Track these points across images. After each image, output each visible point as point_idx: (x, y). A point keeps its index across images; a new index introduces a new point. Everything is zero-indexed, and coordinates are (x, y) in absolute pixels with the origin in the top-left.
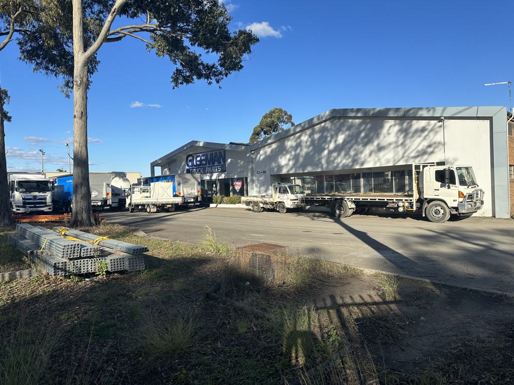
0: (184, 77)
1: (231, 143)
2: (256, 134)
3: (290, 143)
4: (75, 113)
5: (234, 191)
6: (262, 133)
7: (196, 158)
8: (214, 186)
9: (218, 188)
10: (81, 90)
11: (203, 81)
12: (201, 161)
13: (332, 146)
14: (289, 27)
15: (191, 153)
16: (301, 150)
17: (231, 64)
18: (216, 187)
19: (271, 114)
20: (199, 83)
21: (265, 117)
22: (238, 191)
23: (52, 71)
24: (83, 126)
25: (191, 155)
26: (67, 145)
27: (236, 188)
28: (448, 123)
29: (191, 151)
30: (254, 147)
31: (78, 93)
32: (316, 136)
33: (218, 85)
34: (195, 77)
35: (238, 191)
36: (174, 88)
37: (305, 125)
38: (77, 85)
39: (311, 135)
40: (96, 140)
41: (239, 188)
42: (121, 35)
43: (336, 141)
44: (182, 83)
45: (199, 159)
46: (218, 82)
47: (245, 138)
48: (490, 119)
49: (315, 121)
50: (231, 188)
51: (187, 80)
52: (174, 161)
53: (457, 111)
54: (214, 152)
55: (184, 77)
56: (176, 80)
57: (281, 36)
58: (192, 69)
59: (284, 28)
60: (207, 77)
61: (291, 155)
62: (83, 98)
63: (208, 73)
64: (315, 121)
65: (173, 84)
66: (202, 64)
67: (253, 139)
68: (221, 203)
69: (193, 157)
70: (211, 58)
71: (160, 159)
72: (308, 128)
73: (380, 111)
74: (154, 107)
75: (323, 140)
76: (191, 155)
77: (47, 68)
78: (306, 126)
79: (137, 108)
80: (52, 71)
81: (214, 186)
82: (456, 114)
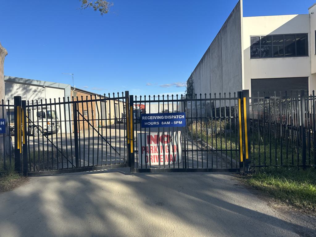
28: (47, 89)
48: (64, 89)
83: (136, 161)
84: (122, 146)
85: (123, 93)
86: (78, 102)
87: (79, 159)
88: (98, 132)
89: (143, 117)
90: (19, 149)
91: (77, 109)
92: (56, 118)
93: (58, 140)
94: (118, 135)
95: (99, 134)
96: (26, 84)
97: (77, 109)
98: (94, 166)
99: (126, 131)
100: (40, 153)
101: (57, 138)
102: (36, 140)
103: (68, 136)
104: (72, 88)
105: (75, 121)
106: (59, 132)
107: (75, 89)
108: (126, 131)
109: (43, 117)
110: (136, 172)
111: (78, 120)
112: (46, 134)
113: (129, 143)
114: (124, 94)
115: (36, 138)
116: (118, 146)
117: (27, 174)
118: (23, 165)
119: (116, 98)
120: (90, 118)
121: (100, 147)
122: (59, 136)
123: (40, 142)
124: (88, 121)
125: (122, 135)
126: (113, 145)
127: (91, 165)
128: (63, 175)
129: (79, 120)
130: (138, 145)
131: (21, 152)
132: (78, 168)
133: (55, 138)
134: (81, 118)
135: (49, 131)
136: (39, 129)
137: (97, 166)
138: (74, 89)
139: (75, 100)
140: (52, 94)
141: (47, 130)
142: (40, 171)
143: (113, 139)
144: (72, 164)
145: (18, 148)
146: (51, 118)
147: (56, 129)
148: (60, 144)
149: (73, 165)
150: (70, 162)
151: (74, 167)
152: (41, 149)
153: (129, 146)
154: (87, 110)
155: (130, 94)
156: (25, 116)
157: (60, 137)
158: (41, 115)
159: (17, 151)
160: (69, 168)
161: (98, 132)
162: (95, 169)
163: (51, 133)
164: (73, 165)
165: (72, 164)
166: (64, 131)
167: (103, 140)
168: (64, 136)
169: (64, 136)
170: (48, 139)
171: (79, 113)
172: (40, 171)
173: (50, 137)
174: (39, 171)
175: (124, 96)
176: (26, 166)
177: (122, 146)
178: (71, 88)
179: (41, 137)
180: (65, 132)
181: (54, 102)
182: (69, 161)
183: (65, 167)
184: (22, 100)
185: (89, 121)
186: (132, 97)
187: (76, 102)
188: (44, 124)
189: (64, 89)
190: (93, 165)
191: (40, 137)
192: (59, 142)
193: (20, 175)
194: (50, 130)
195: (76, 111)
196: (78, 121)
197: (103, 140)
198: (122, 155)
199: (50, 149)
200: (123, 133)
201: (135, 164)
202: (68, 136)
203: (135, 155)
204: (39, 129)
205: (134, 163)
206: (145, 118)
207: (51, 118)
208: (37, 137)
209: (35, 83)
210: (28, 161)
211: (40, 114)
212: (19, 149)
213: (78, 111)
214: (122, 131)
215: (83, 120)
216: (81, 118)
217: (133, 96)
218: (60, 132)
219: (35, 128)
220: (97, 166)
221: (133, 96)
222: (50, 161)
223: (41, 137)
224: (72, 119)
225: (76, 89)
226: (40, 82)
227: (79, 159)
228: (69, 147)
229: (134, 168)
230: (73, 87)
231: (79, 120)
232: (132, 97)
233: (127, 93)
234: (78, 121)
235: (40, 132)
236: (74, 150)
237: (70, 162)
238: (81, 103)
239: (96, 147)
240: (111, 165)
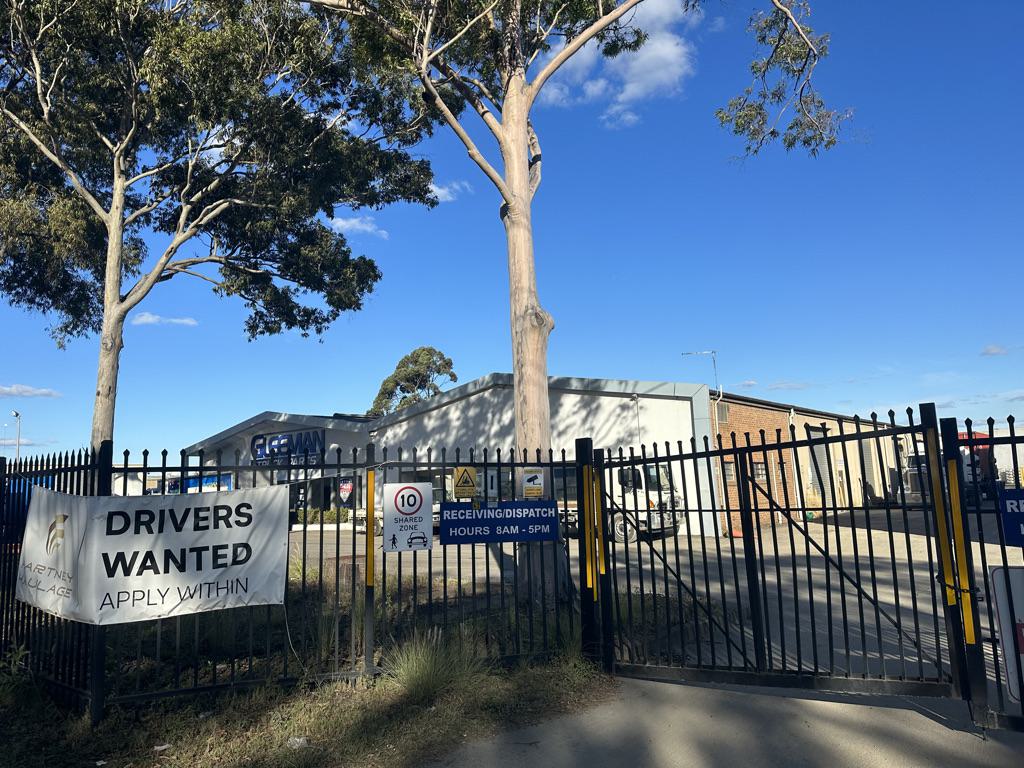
0: (266, 323)
1: (337, 416)
2: (387, 393)
3: (430, 423)
4: (100, 389)
5: (339, 501)
6: (398, 391)
7: (270, 443)
8: (302, 491)
9: (309, 496)
10: (111, 355)
11: (297, 330)
12: (280, 446)
13: (495, 428)
14: (466, 184)
15: (261, 433)
16: (447, 435)
17: (344, 301)
18: (305, 494)
19: (414, 359)
20: (291, 335)
21: (403, 364)
22: (345, 500)
23: (39, 305)
24: (110, 408)
25: (261, 437)
26: (17, 415)
27: (342, 495)
28: (643, 401)
29: (260, 429)
30: (375, 420)
31: (107, 360)
32: (472, 413)
33: (319, 337)
34: (283, 325)
35: (345, 500)
36: (250, 340)
37: (455, 395)
38: (107, 349)
39: (465, 410)
40: (44, 391)
41: (347, 495)
42: (171, 272)
43: (500, 421)
44: (262, 333)
45: (275, 443)
46: (319, 331)
47: (360, 404)
48: (689, 399)
49: (471, 389)
50: (332, 495)
51: (271, 329)
52: (228, 446)
53: (651, 387)
54: (303, 432)
55: (266, 323)
56: (253, 328)
57: (450, 198)
58: (283, 312)
59: (456, 186)
60: (304, 325)
61: (434, 440)
62: (113, 367)
63: (309, 318)
64: (471, 389)
65: (248, 334)
66: (297, 306)
67: (378, 402)
68: (312, 523)
69: (265, 440)
70: (312, 300)
71: (202, 443)
72: (458, 400)
73: (558, 381)
74: (183, 325)
75: (481, 418)
76: (261, 437)
77: (31, 301)
78: (457, 397)
79: (146, 326)
80: (39, 305)
81: (302, 491)
82: (652, 390)
83: (991, 676)
84: (925, 607)
85: (910, 411)
86: (750, 449)
87: (766, 640)
88: (808, 540)
89: (1008, 502)
90: (592, 589)
91: (749, 474)
92: (672, 488)
93: (682, 559)
94: (901, 555)
95: (805, 533)
96: (592, 392)
97: (749, 474)
98: (821, 674)
99: (933, 540)
100: (634, 602)
101: (677, 552)
102: (620, 553)
103: (711, 546)
104: (712, 393)
105: (746, 511)
106: (682, 530)
107: (724, 397)
108: (933, 540)
109: (637, 485)
110: (1000, 725)
111: (753, 507)
112: (648, 536)
113: (952, 601)
114: (914, 415)
115: (620, 546)
116: (906, 602)
117: (614, 667)
118: (602, 635)
119: (885, 433)
120: (796, 503)
121: (836, 597)
122: (683, 545)
123: (630, 562)
124: (787, 512)
125: (920, 554)
126: (886, 596)
127: (808, 666)
128: (714, 687)
129: (757, 510)
130: (991, 592)
131: (595, 599)
132: (762, 673)
133: (671, 553)
134: (763, 503)
135: (653, 527)
136: (626, 519)
137: (829, 674)
138: (719, 396)
139: (741, 443)
140: (664, 425)
141: (648, 523)
142: (647, 665)
143: (882, 568)
144: (744, 654)
145: (589, 585)
146: (659, 489)
147: (675, 522)
148: (686, 574)
149: (746, 661)
150: (737, 648)
151: (749, 666)
152: (648, 589)
153: (954, 613)
154: (762, 461)
155: (941, 414)
156: (603, 494)
157: (687, 548)
158: (630, 482)
159: (586, 592)
160: (735, 668)
161: (808, 540)
162: (823, 683)
163: (662, 534)
164: (746, 661)
165: (744, 654)
166: (695, 530)
167: (836, 561)
168: (697, 546)
169: (697, 546)
170: (652, 550)
171: (755, 486)
172: (647, 665)
173: (657, 545)
174: (645, 663)
175: (917, 421)
176: (609, 639)
177: (925, 607)
178: (711, 394)
179: (633, 546)
180: (699, 533)
181: (677, 453)
182: (734, 645)
183: (722, 661)
184: (594, 448)
185: (792, 512)
186: (949, 424)
187: (743, 451)
188: (639, 501)
189: (689, 399)
190: (816, 667)
191: (630, 545)
192: (685, 566)
193: (596, 668)
194: (656, 525)
195: (745, 480)
196: (754, 513)
197: (836, 561)
198: (928, 641)
199: (660, 588)
200: (921, 547)
201: (992, 691)
202: (711, 546)
203: (987, 648)
204: (626, 519)
205: (985, 691)
206: (1018, 507)
207: (659, 489)
208: (623, 545)
209: (611, 387)
210: (615, 624)
211: (627, 476)
212: (592, 589)
213: (752, 479)
214: (919, 542)
215: (771, 510)
216: (763, 503)
217: (954, 420)
218: (686, 533)
219: (615, 516)
220: (829, 674)
221: (954, 420)
222: (675, 629)
223: (633, 546)
224: (735, 504)
225: (726, 396)
226: (627, 383)
227: (766, 640)
228: (715, 588)
229: (984, 708)
230: (714, 389)
231: (757, 510)
232: (949, 424)
233: (928, 410)
234: (754, 513)
235: (629, 527)
236: (748, 602)
237: (737, 648)
238: (762, 453)
239: (820, 596)
240: (886, 680)
